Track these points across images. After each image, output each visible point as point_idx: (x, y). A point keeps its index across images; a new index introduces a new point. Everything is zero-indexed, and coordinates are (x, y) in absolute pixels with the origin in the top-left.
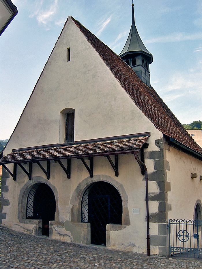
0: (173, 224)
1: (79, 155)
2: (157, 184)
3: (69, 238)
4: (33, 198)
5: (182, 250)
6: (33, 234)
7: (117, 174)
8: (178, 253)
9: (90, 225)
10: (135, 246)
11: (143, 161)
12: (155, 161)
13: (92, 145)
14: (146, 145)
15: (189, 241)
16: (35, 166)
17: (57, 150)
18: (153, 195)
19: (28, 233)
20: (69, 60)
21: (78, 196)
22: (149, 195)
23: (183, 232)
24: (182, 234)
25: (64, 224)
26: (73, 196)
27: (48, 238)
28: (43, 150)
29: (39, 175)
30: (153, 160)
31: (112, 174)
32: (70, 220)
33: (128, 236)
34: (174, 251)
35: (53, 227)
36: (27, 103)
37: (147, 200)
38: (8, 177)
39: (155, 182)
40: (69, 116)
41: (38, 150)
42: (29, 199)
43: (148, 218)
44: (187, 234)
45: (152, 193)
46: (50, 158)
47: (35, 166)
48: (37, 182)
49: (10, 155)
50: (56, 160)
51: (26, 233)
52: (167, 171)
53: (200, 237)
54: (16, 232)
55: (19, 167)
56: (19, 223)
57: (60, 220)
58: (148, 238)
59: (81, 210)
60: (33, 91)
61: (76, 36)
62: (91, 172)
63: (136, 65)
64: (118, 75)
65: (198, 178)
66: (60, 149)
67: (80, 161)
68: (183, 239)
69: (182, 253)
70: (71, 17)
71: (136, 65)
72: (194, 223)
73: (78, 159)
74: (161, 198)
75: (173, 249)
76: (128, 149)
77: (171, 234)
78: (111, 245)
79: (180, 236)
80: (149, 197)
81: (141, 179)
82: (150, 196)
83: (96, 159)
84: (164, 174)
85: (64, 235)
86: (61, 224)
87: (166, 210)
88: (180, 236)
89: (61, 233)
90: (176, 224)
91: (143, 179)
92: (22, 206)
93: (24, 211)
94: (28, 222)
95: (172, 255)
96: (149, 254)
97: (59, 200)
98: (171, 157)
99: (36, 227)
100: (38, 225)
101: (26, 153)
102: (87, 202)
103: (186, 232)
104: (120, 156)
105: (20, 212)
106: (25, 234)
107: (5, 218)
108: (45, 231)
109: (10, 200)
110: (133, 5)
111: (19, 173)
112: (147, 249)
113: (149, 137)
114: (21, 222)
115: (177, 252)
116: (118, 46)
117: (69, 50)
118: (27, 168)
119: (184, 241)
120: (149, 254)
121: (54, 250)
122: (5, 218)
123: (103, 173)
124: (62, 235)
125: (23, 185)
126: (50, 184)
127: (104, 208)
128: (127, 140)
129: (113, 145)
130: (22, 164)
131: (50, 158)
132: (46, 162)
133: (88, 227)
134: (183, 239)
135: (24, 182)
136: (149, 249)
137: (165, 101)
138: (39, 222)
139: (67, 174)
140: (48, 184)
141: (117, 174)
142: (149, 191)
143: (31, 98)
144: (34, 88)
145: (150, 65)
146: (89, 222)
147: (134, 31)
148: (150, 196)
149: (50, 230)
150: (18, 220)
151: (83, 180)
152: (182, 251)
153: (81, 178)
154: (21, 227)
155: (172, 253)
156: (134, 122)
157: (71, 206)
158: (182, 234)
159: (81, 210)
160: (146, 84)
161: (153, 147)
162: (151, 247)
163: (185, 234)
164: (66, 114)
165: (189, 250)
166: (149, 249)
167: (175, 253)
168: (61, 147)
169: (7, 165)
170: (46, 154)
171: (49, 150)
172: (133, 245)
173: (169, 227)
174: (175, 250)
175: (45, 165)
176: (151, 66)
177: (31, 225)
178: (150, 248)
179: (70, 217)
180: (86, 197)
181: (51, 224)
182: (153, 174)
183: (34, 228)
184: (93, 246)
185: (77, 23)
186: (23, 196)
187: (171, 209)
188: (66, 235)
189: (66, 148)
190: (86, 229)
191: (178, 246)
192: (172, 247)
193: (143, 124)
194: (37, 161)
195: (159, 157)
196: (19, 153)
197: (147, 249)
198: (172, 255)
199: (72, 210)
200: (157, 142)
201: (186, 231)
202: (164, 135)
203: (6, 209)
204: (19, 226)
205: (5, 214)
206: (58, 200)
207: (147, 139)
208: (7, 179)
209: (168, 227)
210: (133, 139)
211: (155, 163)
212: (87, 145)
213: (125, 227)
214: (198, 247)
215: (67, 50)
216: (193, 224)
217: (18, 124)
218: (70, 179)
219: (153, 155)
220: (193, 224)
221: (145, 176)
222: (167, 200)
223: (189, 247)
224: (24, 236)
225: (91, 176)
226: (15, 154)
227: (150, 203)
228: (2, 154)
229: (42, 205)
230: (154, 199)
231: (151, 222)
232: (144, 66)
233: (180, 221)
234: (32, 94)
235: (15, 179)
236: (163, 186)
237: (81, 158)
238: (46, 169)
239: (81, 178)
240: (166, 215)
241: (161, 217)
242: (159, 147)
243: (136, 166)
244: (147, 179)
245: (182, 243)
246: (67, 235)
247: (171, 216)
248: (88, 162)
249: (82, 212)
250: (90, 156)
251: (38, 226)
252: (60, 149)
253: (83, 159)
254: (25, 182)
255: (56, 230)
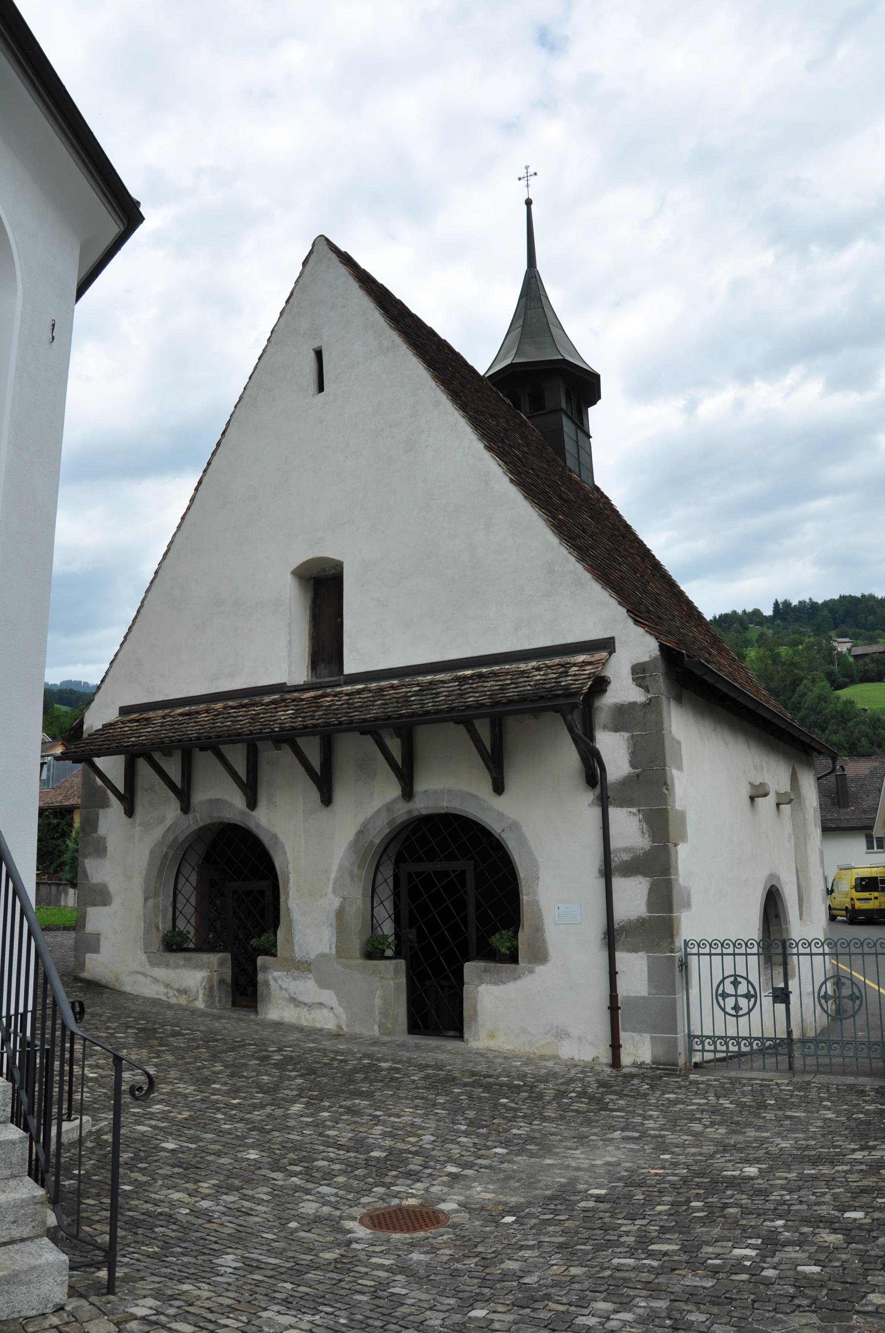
0: (798, 954)
1: (365, 720)
2: (641, 816)
3: (332, 1014)
4: (193, 878)
5: (733, 1043)
6: (200, 1004)
7: (499, 788)
8: (719, 1055)
9: (404, 967)
10: (568, 1035)
11: (592, 738)
12: (633, 736)
13: (410, 685)
14: (600, 684)
15: (756, 1012)
16: (204, 762)
17: (285, 706)
18: (625, 857)
19: (183, 1001)
20: (321, 388)
21: (360, 866)
22: (612, 856)
23: (735, 984)
24: (730, 989)
25: (312, 967)
26: (341, 867)
27: (252, 1016)
28: (233, 708)
29: (218, 795)
30: (627, 735)
31: (482, 787)
32: (334, 951)
33: (538, 1009)
34: (703, 1050)
35: (270, 977)
36: (171, 542)
37: (607, 872)
38: (105, 804)
39: (634, 810)
40: (323, 586)
41: (213, 706)
42: (182, 880)
43: (613, 937)
44: (751, 988)
45: (626, 850)
46: (262, 733)
47: (204, 762)
48: (209, 821)
49: (111, 724)
50: (284, 741)
51: (173, 1001)
52: (675, 772)
53: (794, 998)
54: (137, 997)
55: (144, 768)
56: (148, 966)
57: (299, 954)
58: (614, 1007)
59: (373, 915)
60: (192, 500)
61: (345, 307)
62: (406, 776)
63: (544, 409)
64: (496, 441)
65: (771, 799)
66: (293, 700)
67: (369, 741)
68: (736, 1008)
69: (740, 1054)
70: (327, 239)
71: (544, 409)
72: (761, 951)
73: (362, 733)
74: (656, 865)
75: (702, 1043)
76: (542, 697)
77: (694, 991)
78: (483, 1033)
79: (725, 995)
80: (613, 865)
81: (583, 808)
82: (616, 859)
83: (424, 735)
84: (665, 784)
85: (310, 1006)
86: (302, 967)
87: (675, 909)
88: (725, 995)
89: (300, 999)
90: (710, 954)
91: (590, 801)
92: (156, 906)
93: (164, 922)
94: (181, 963)
95: (695, 1063)
96: (616, 1062)
97: (291, 882)
98: (682, 727)
99: (210, 979)
100: (215, 974)
101: (171, 716)
102: (392, 888)
103: (744, 982)
104: (512, 725)
105: (150, 926)
106: (170, 1006)
107: (96, 950)
108: (244, 990)
109: (113, 888)
110: (529, 203)
111: (146, 790)
112: (609, 1008)
113: (610, 654)
114: (153, 964)
115: (715, 1051)
116: (482, 355)
117: (319, 354)
118: (174, 770)
119: (741, 1013)
120: (616, 1062)
121: (282, 1055)
122: (96, 950)
123: (451, 784)
124: (305, 1004)
125: (157, 833)
126: (258, 825)
127: (451, 908)
128: (533, 668)
129: (485, 684)
130: (157, 756)
131: (262, 733)
132: (177, 756)
133: (396, 972)
134: (736, 1008)
135: (162, 820)
136: (615, 1046)
137: (649, 545)
138: (221, 963)
139: (320, 789)
140: (252, 826)
141: (499, 788)
142: (614, 844)
143: (152, 589)
144: (196, 489)
145: (589, 409)
146: (398, 955)
147: (532, 291)
148: (616, 860)
149: (261, 989)
150: (144, 957)
151: (378, 811)
152: (732, 1048)
153: (368, 804)
154: (156, 980)
155: (697, 1058)
156: (531, 599)
157: (336, 903)
158: (730, 989)
159: (373, 915)
160: (580, 477)
161: (623, 690)
162: (624, 1036)
163: (730, 1002)
164: (310, 579)
165: (757, 1044)
166: (615, 1046)
167: (709, 1056)
168: (296, 694)
169: (99, 762)
170: (242, 721)
171: (254, 705)
172: (562, 1034)
173: (686, 967)
174: (719, 1048)
175: (238, 757)
176: (594, 413)
177: (191, 973)
178: (621, 1043)
179: (334, 940)
180: (388, 871)
181: (265, 969)
182: (626, 782)
183: (202, 983)
184: (417, 1041)
185: (346, 260)
186: (160, 872)
187: (688, 905)
188: (321, 1004)
189: (315, 698)
190: (392, 983)
191: (720, 1032)
192: (697, 1037)
193: (587, 611)
194: (212, 744)
195: (639, 722)
196: (146, 719)
197: (609, 1008)
198: (696, 1065)
199: (340, 914)
200: (640, 673)
201: (746, 979)
202: (662, 647)
203: (98, 919)
204: (149, 979)
205: (97, 937)
206: (287, 882)
207: (604, 663)
208: (101, 811)
209: (684, 966)
210: (557, 661)
211: (635, 746)
212: (392, 687)
213: (531, 971)
214: (790, 1033)
215: (313, 354)
216: (758, 954)
217: (139, 618)
218: (328, 809)
219: (623, 717)
220: (758, 954)
221: (598, 790)
222: (677, 874)
223: (756, 1033)
224: (168, 1012)
225: (408, 793)
226: (130, 721)
227: (618, 883)
228: (82, 723)
229: (230, 898)
230: (633, 868)
231: (622, 951)
232: (569, 414)
233: (746, 944)
234: (189, 508)
235: (130, 812)
236: (661, 824)
237: (371, 729)
238: (242, 772)
239: (368, 804)
240: (675, 926)
241: (658, 928)
242: (647, 690)
243: (569, 757)
244: (604, 802)
245: (731, 1020)
246: (321, 1004)
247: (690, 926)
248: (394, 745)
249: (375, 921)
250: (400, 719)
251: (215, 977)
252: (293, 700)
253: (473, 725)
254: (169, 822)
255: (284, 987)
